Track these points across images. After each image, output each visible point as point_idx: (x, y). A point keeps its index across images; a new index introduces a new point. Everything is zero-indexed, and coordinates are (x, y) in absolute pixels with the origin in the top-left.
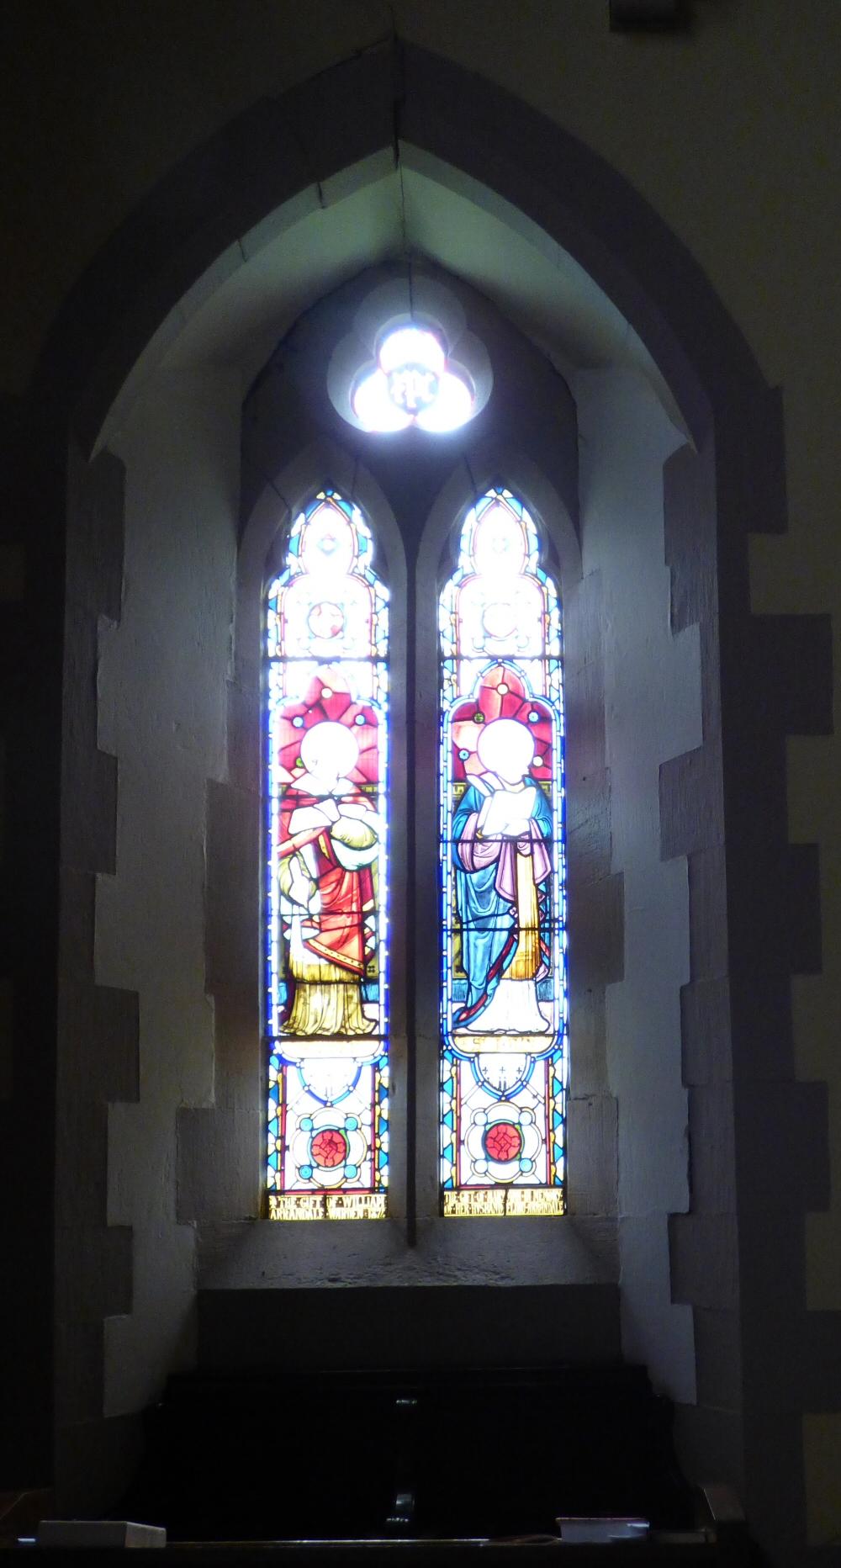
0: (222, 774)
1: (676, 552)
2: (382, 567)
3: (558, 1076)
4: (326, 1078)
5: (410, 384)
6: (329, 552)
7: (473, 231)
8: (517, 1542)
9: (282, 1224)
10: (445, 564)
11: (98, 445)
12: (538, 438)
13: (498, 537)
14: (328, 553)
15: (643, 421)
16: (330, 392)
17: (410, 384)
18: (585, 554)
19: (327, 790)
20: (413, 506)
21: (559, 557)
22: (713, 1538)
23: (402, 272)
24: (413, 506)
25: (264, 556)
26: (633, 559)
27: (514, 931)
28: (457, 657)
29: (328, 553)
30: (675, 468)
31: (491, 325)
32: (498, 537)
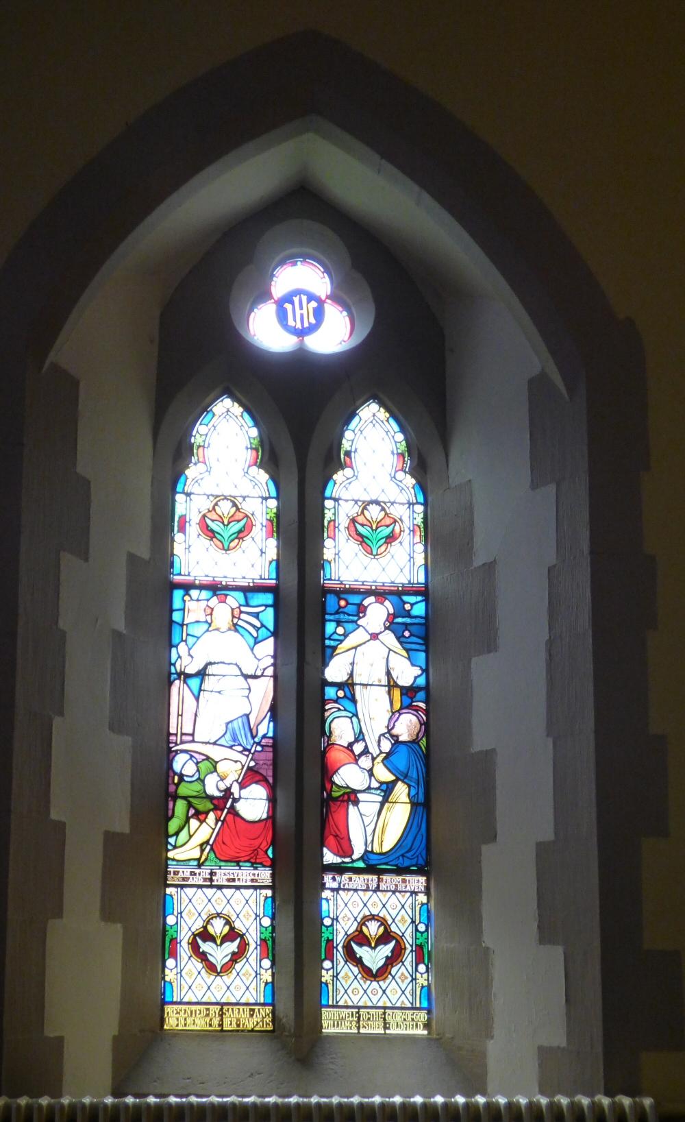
0: (144, 552)
1: (542, 469)
4: (216, 901)
5: (300, 310)
6: (226, 448)
7: (361, 181)
9: (176, 1034)
11: (52, 357)
12: (412, 361)
13: (373, 443)
15: (505, 346)
16: (234, 317)
17: (300, 310)
18: (452, 458)
19: (222, 692)
20: (301, 419)
23: (304, 212)
24: (301, 419)
25: (176, 454)
26: (492, 464)
28: (348, 686)
30: (538, 385)
31: (375, 265)
32: (373, 443)
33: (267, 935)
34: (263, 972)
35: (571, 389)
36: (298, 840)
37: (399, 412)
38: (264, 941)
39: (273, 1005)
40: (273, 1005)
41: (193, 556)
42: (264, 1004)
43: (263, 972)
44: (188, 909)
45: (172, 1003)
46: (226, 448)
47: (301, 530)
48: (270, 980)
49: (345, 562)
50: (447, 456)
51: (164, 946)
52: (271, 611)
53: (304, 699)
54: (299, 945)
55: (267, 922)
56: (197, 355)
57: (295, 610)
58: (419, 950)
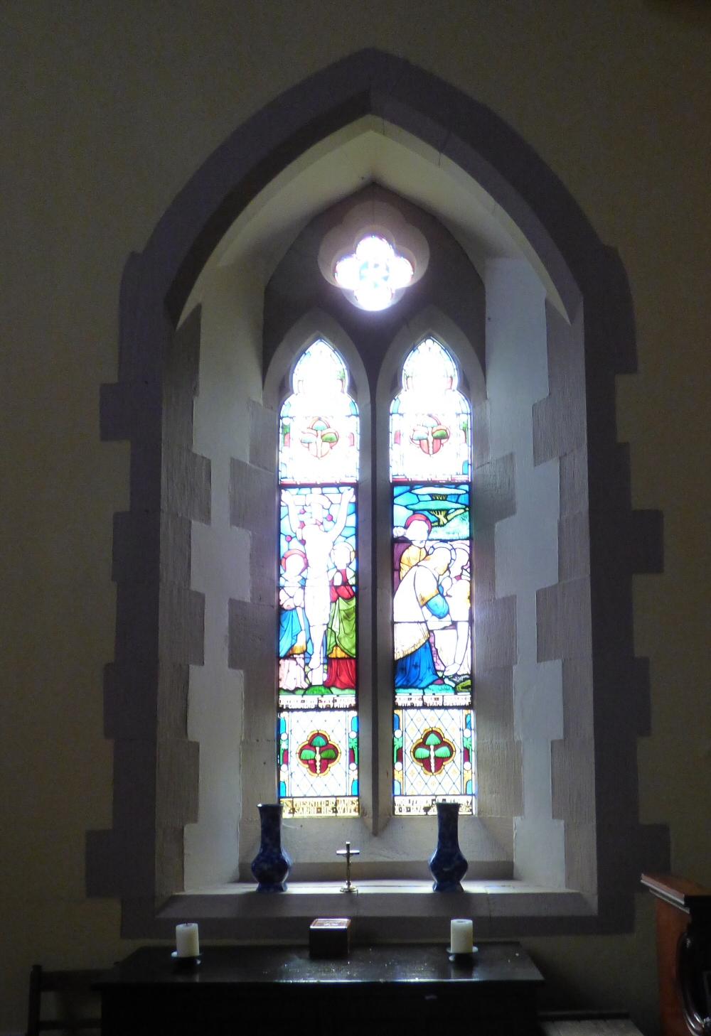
2: (354, 389)
3: (290, 639)
4: (316, 715)
5: (374, 273)
6: (320, 372)
8: (417, 980)
10: (394, 386)
12: (452, 300)
13: (430, 369)
14: (333, 417)
15: (524, 285)
17: (374, 273)
18: (488, 386)
20: (375, 355)
21: (472, 383)
22: (448, 951)
23: (375, 201)
24: (375, 355)
27: (574, 457)
29: (333, 417)
32: (430, 369)
33: (354, 744)
34: (351, 772)
35: (572, 318)
36: (375, 673)
37: (453, 347)
38: (352, 750)
39: (358, 796)
40: (358, 796)
41: (293, 461)
42: (352, 796)
43: (351, 772)
44: (297, 729)
45: (285, 797)
46: (320, 372)
47: (375, 442)
48: (356, 778)
49: (404, 461)
50: (485, 376)
51: (279, 757)
52: (354, 538)
53: (380, 555)
54: (378, 757)
55: (354, 735)
56: (295, 305)
57: (370, 641)
58: (466, 753)
